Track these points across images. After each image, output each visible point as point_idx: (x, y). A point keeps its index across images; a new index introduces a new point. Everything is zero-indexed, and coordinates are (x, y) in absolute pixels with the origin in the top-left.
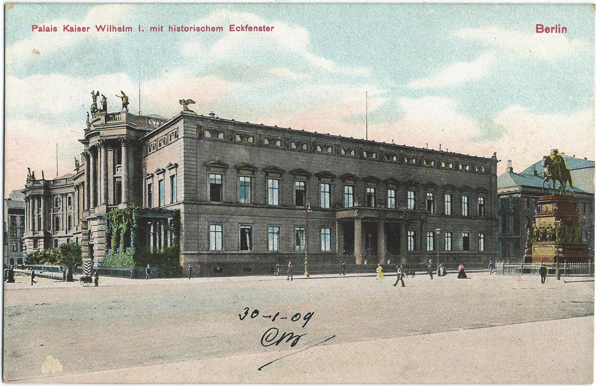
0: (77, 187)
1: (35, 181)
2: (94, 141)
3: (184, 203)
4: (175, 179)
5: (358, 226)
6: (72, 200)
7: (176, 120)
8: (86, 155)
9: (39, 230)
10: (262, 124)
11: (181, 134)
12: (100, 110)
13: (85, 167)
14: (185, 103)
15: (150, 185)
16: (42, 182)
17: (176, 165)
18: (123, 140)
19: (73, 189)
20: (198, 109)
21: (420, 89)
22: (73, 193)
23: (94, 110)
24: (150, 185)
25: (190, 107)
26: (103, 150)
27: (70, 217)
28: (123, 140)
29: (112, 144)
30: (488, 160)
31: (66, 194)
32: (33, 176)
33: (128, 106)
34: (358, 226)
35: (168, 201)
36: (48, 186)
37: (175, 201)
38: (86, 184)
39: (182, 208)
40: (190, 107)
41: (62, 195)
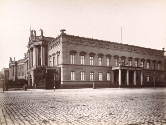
0: (25, 62)
1: (12, 62)
2: (32, 46)
3: (63, 64)
4: (59, 56)
5: (120, 72)
6: (23, 67)
7: (59, 37)
8: (29, 51)
9: (14, 76)
10: (88, 38)
11: (61, 41)
12: (33, 36)
13: (29, 55)
14: (62, 31)
15: (50, 62)
16: (14, 62)
17: (60, 52)
18: (40, 44)
19: (24, 63)
20: (67, 33)
21: (98, 97)
22: (24, 65)
23: (32, 35)
24: (50, 62)
25: (64, 32)
26: (35, 48)
27: (23, 72)
28: (40, 44)
29: (38, 47)
30: (160, 51)
31: (22, 65)
32: (12, 60)
33: (43, 34)
34: (120, 72)
35: (56, 64)
36: (16, 63)
37: (59, 64)
38: (29, 62)
39: (62, 66)
40: (64, 32)
41: (20, 65)
